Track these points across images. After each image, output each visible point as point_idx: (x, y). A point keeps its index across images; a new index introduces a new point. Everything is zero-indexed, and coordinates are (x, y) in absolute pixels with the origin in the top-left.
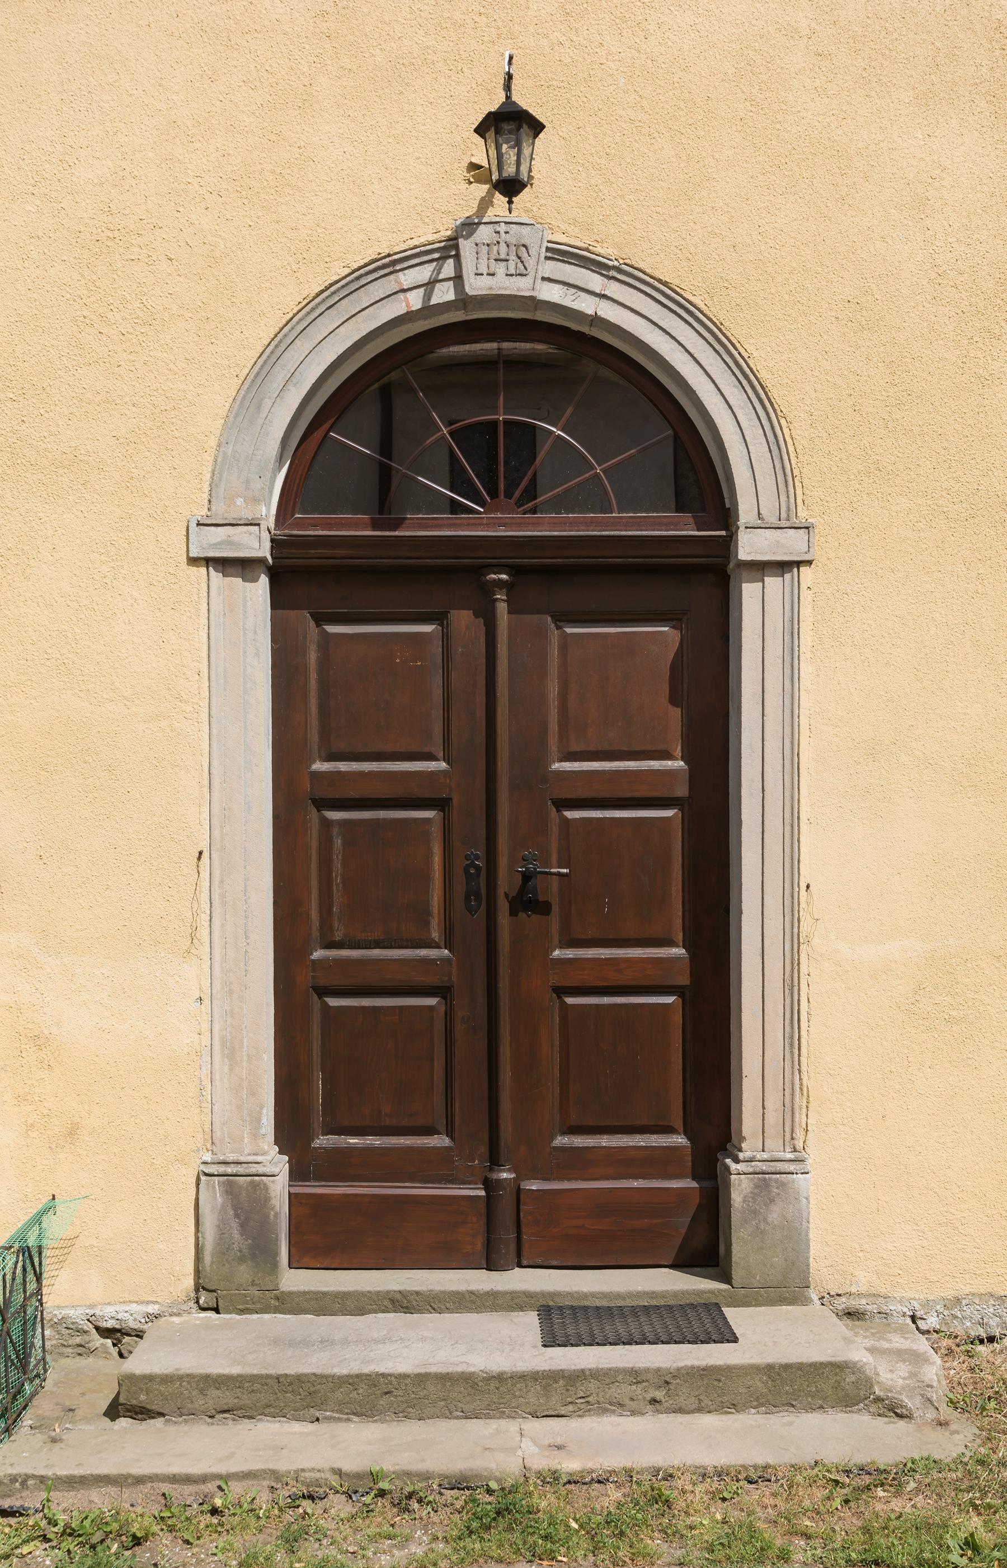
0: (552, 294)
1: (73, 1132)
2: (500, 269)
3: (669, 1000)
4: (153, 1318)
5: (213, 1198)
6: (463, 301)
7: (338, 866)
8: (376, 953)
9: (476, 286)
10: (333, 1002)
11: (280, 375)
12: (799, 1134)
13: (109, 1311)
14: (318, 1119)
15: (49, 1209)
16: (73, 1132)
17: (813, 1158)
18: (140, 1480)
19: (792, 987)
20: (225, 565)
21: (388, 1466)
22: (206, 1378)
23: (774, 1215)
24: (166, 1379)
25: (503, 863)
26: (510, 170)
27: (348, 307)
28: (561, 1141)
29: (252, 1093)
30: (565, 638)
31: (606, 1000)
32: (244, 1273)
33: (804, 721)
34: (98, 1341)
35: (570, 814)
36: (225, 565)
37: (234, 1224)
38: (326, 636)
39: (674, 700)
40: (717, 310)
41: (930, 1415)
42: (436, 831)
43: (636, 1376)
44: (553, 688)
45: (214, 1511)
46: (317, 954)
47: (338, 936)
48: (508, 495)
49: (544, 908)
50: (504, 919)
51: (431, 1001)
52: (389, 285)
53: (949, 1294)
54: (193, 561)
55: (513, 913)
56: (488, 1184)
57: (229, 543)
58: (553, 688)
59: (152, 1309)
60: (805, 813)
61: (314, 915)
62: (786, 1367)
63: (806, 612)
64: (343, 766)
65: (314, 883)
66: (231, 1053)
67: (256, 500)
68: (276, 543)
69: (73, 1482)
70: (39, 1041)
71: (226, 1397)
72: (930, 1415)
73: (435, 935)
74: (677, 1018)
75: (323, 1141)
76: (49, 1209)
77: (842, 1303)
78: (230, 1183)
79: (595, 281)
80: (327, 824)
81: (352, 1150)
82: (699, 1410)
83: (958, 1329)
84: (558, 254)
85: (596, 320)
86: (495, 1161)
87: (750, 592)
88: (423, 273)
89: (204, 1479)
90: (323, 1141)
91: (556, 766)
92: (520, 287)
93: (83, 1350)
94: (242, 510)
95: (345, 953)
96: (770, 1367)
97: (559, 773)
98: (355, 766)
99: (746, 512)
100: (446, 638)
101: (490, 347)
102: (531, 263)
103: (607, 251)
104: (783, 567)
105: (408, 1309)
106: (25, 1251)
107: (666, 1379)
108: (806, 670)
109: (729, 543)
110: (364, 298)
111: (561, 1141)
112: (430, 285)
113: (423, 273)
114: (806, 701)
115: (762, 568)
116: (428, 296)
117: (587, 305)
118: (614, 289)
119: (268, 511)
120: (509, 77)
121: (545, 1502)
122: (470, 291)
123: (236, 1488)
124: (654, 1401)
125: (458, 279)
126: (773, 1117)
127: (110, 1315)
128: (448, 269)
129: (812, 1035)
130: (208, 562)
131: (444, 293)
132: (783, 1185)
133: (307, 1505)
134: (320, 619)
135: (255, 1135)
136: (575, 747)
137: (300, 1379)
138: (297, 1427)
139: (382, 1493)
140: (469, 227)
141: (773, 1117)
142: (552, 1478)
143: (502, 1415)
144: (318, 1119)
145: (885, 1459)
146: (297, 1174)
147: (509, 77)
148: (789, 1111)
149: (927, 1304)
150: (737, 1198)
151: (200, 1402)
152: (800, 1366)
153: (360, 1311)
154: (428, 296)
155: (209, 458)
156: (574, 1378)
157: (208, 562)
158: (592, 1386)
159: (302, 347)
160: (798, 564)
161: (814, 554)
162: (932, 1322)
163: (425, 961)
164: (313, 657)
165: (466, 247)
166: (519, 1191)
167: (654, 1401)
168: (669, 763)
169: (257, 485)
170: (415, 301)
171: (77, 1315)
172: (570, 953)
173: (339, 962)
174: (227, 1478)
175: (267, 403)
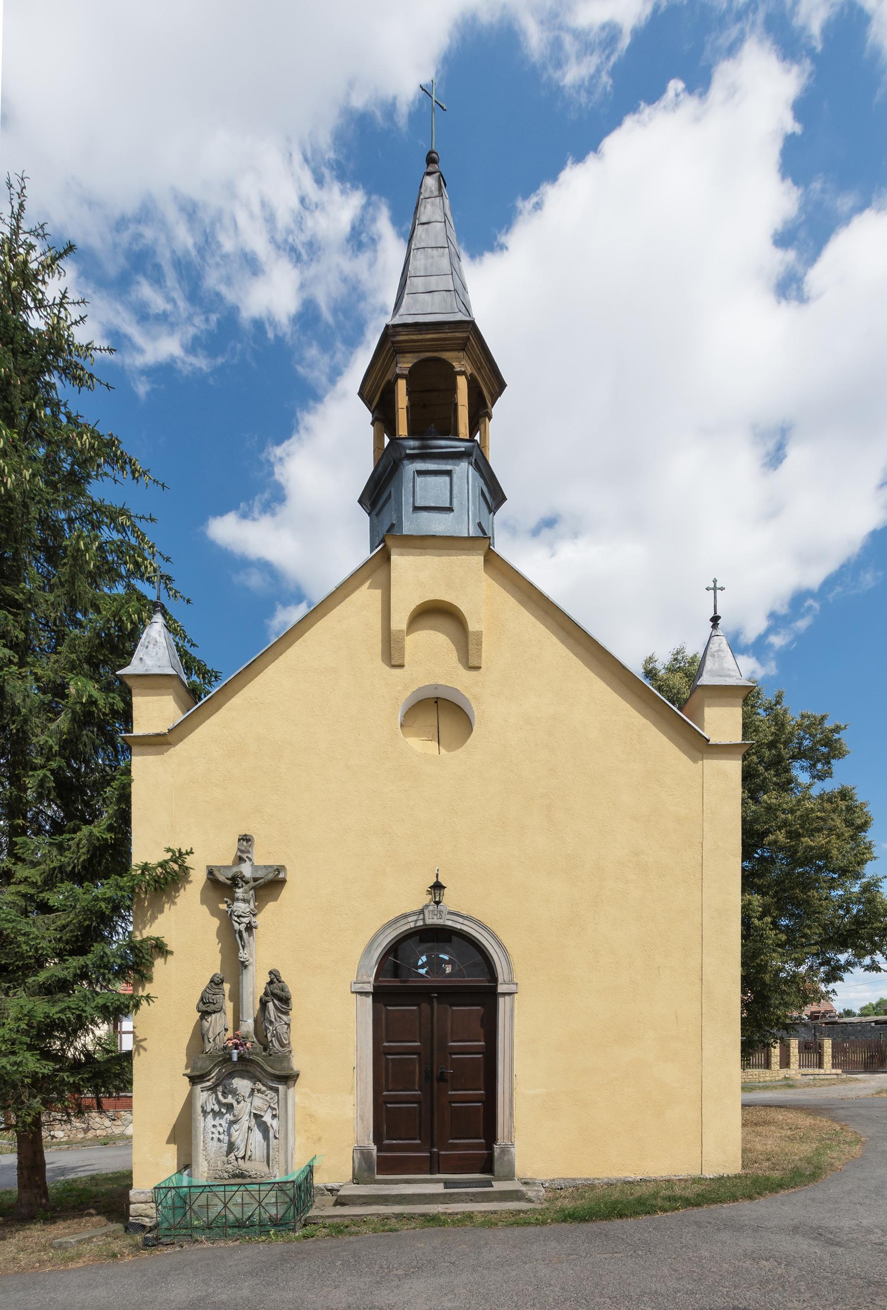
0: (449, 923)
1: (320, 1139)
2: (435, 917)
3: (480, 1104)
4: (341, 1186)
5: (357, 1156)
6: (425, 925)
7: (390, 1071)
8: (401, 1093)
9: (429, 921)
10: (389, 1106)
11: (376, 944)
12: (513, 1138)
13: (330, 1184)
14: (385, 1136)
15: (314, 1158)
16: (320, 1139)
17: (516, 1144)
18: (345, 1216)
19: (511, 1101)
20: (361, 993)
21: (406, 1212)
22: (360, 1195)
23: (506, 1158)
24: (349, 1196)
25: (435, 1069)
26: (437, 899)
27: (394, 926)
28: (450, 1141)
29: (368, 1129)
30: (453, 1011)
31: (463, 1105)
32: (366, 1174)
33: (515, 1034)
34: (327, 1192)
35: (453, 1056)
36: (361, 993)
37: (363, 1162)
38: (388, 1010)
39: (482, 1026)
40: (493, 928)
41: (539, 1201)
42: (417, 1061)
43: (467, 1194)
44: (449, 1024)
45: (365, 1221)
46: (385, 1093)
47: (390, 1088)
48: (437, 973)
49: (446, 1081)
50: (435, 1084)
51: (416, 1105)
52: (405, 921)
53: (552, 1178)
54: (353, 992)
55: (438, 1082)
56: (430, 1152)
57: (362, 988)
58: (449, 1024)
59: (341, 1184)
60: (515, 1056)
61: (384, 1083)
62: (504, 1191)
63: (516, 1005)
64: (392, 1044)
65: (384, 1075)
66: (362, 1119)
67: (369, 976)
68: (374, 986)
69: (329, 1217)
70: (311, 1116)
71: (364, 1200)
72: (539, 1201)
73: (417, 1088)
74: (482, 1109)
75: (386, 1142)
76: (314, 1158)
77: (523, 1181)
78: (362, 1153)
79: (461, 920)
80: (387, 1059)
81: (394, 1144)
82: (482, 1202)
83: (553, 1186)
84: (450, 913)
85: (461, 929)
86: (433, 1146)
87: (501, 1000)
88: (415, 918)
89: (361, 1215)
90: (386, 1142)
91: (450, 1044)
92: (441, 922)
93: (323, 1195)
94: (365, 979)
95: (392, 1093)
96: (500, 1191)
97: (451, 1046)
98: (395, 1044)
99: (500, 979)
100: (420, 1011)
101: (434, 343)
102: (443, 915)
103: (464, 913)
104: (510, 994)
105: (409, 1183)
106: (310, 1166)
107: (474, 1194)
108: (516, 1020)
109: (496, 987)
110: (399, 924)
111: (450, 1141)
112: (416, 921)
113: (415, 918)
114: (515, 1028)
115: (504, 994)
116: (416, 924)
117: (458, 926)
118: (466, 922)
119: (372, 979)
120: (437, 875)
121: (442, 1218)
122: (427, 923)
123: (369, 1217)
124: (471, 1200)
125: (424, 919)
126: (506, 1134)
127: (330, 1185)
128: (421, 917)
129: (516, 1113)
130: (356, 993)
131: (420, 923)
132: (508, 1151)
133: (386, 1220)
134: (386, 1005)
135: (368, 1140)
136: (455, 1039)
137: (383, 1196)
138: (382, 1207)
139: (404, 1217)
140: (427, 906)
141: (506, 1134)
142: (445, 1213)
143: (433, 1204)
144: (385, 1136)
145: (524, 1209)
146: (379, 1150)
147: (437, 875)
148: (510, 1133)
149: (546, 1181)
150: (496, 1154)
151: (358, 1201)
152: (507, 1191)
153: (397, 1184)
154: (416, 924)
155: (357, 966)
156: (451, 1194)
157: (356, 993)
158: (456, 1196)
159: (382, 937)
160: (514, 993)
161: (518, 991)
162: (547, 1185)
163: (414, 1095)
164: (384, 1016)
165: (426, 912)
166: (439, 1154)
167: (471, 1200)
168: (480, 1043)
169: (369, 972)
170: (412, 925)
171: (321, 1186)
172: (453, 1093)
173: (390, 1095)
174: (367, 1215)
175: (372, 952)
